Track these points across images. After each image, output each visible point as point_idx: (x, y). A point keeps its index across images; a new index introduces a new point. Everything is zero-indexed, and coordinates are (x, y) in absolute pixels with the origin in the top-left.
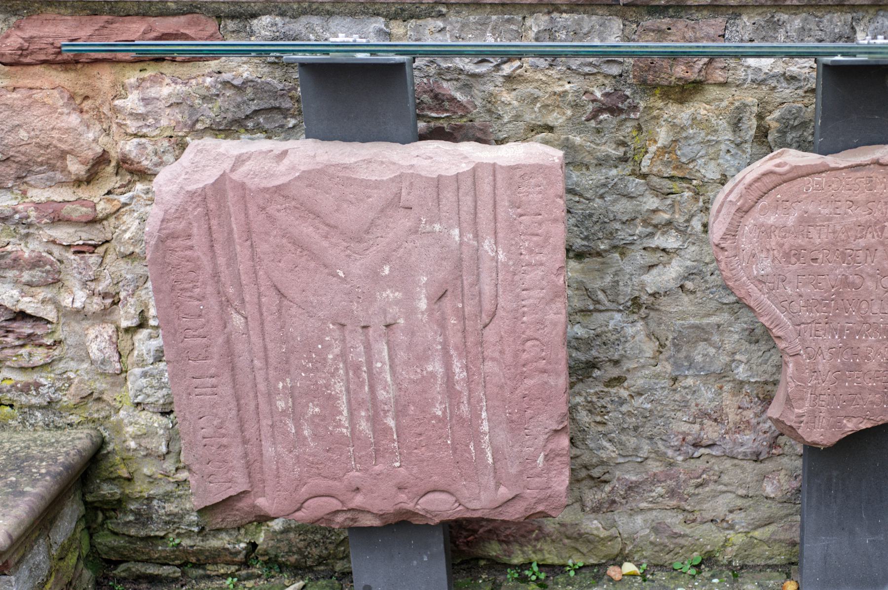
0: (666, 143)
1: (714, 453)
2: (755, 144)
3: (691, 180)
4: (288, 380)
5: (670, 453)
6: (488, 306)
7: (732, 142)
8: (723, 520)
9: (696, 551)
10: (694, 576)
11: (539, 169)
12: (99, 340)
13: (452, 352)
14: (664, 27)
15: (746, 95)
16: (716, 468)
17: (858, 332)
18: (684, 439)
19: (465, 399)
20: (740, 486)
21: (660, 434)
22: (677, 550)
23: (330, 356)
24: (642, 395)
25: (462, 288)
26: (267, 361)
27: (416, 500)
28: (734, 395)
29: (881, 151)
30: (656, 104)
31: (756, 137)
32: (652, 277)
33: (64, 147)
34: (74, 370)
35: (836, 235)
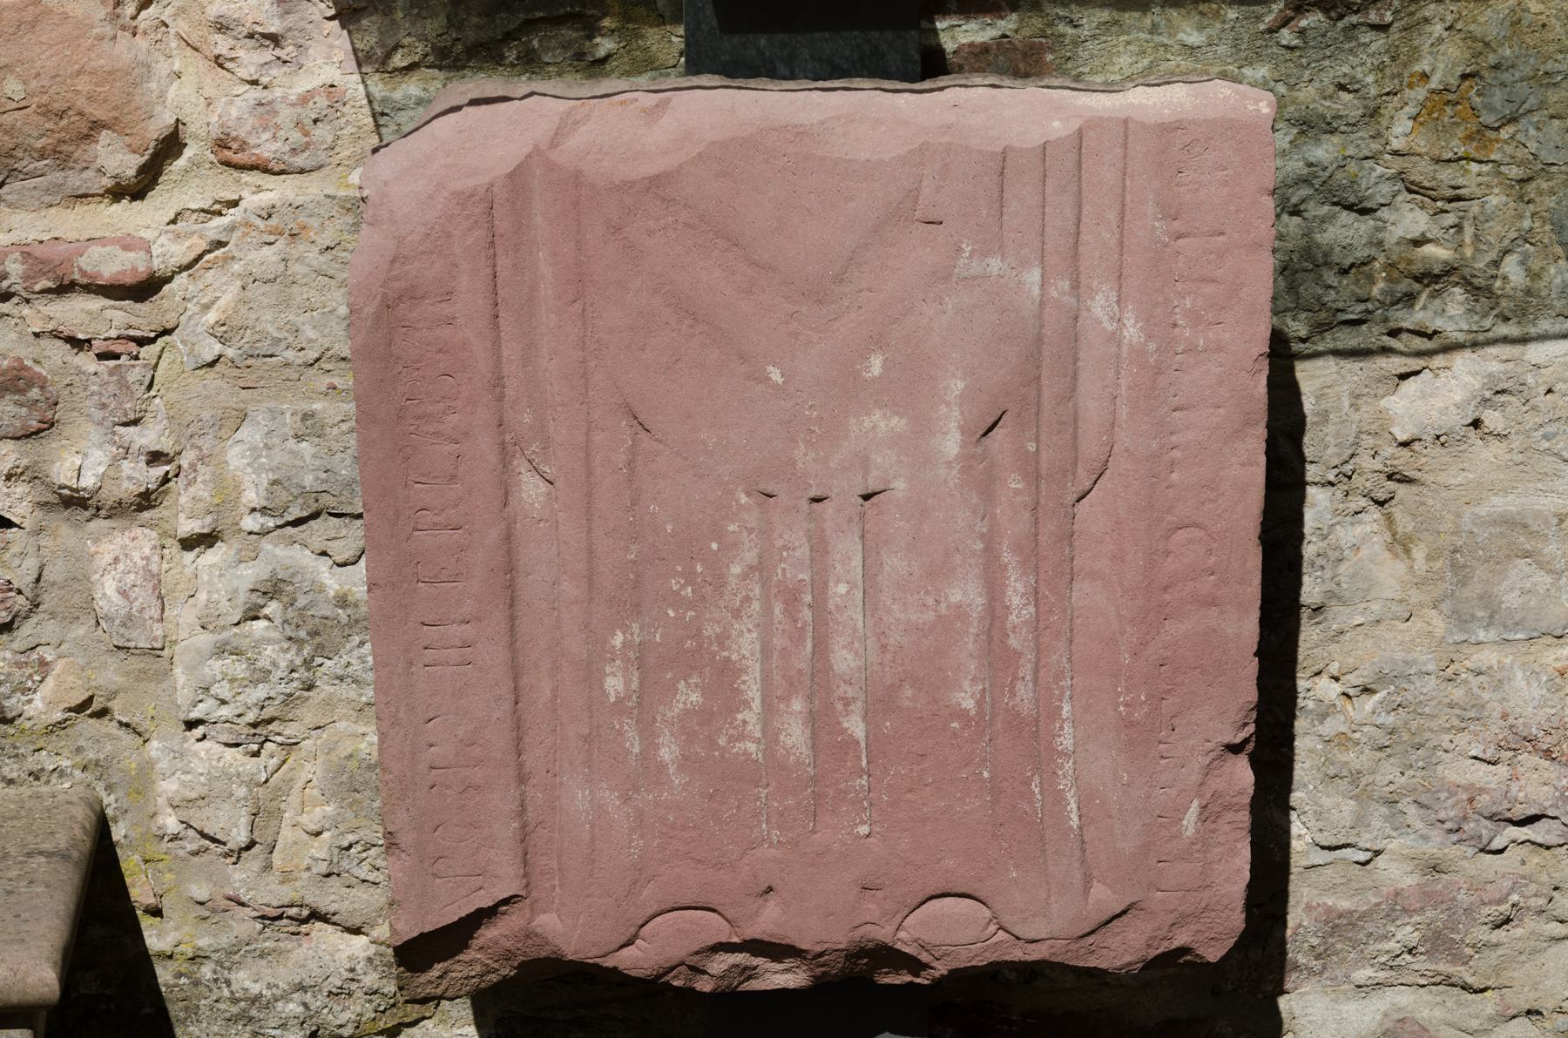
4: (636, 627)
6: (1091, 448)
11: (1230, 128)
12: (121, 567)
13: (1006, 557)
18: (1471, 800)
19: (1026, 671)
23: (736, 569)
25: (1039, 405)
26: (590, 583)
27: (899, 918)
33: (100, 114)
34: (54, 641)
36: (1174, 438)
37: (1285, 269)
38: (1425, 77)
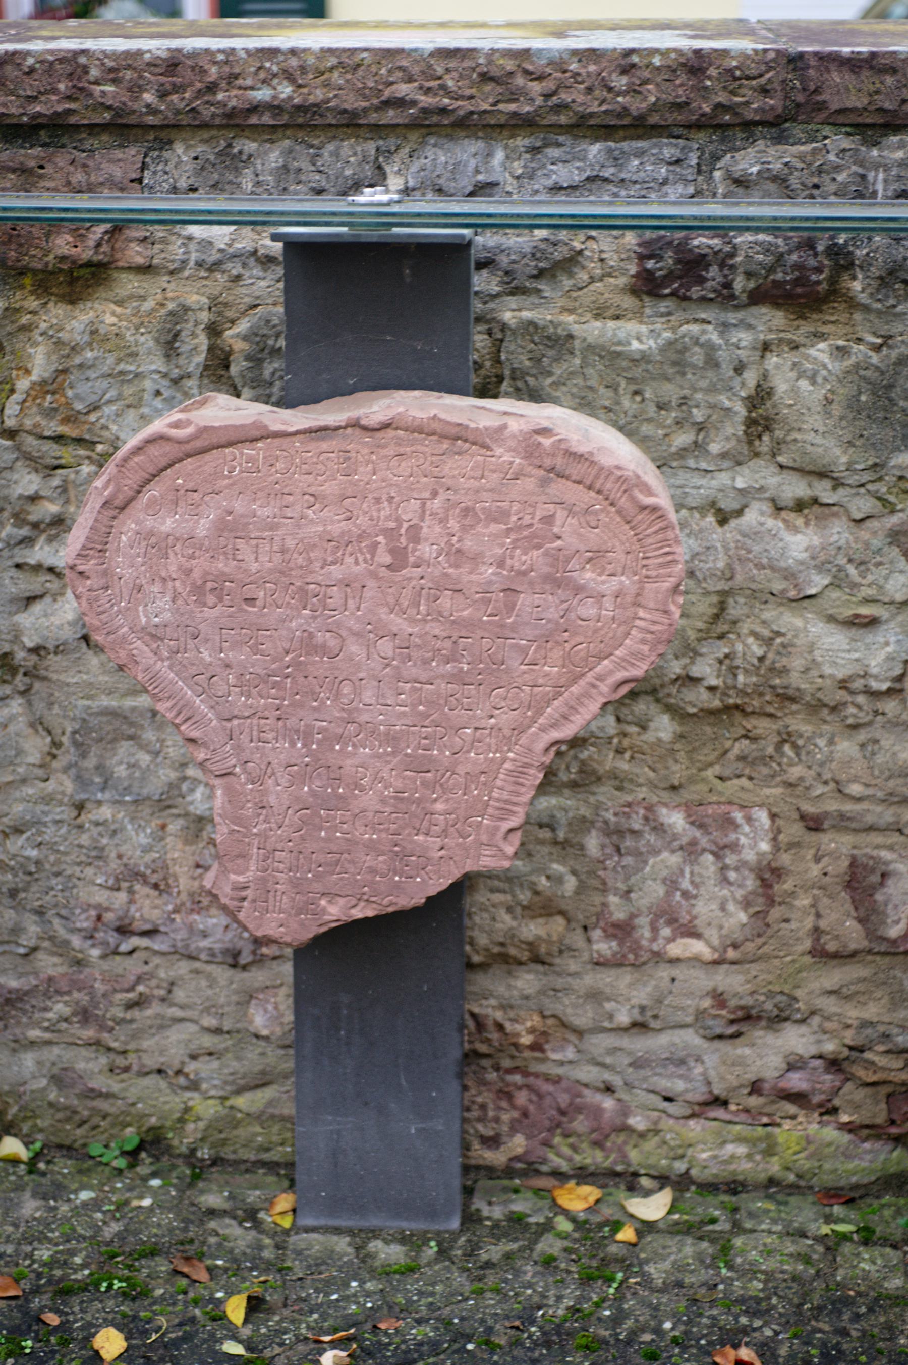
0: (46, 375)
1: (156, 947)
2: (206, 381)
3: (94, 443)
5: (76, 941)
7: (165, 376)
8: (179, 1072)
9: (129, 1125)
10: (120, 1172)
14: (32, 164)
15: (188, 289)
16: (162, 975)
17: (339, 738)
18: (99, 918)
20: (207, 1010)
21: (56, 906)
22: (96, 1120)
24: (22, 832)
28: (187, 842)
29: (385, 402)
30: (26, 304)
31: (206, 367)
32: (32, 619)
35: (287, 556)
37: (768, 393)
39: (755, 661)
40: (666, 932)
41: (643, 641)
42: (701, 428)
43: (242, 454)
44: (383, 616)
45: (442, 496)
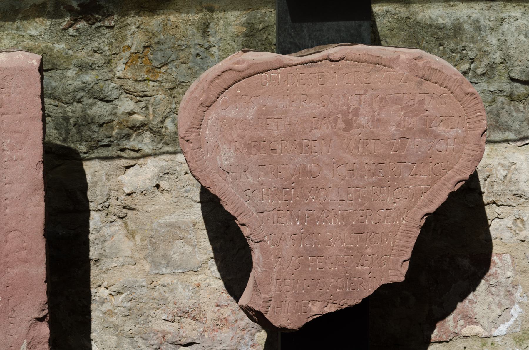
11: (21, 70)
17: (319, 219)
18: (164, 337)
36: (6, 195)
38: (129, 47)
39: (502, 178)
40: (462, 322)
41: (468, 160)
42: (472, 61)
43: (270, 76)
44: (341, 155)
45: (370, 92)
